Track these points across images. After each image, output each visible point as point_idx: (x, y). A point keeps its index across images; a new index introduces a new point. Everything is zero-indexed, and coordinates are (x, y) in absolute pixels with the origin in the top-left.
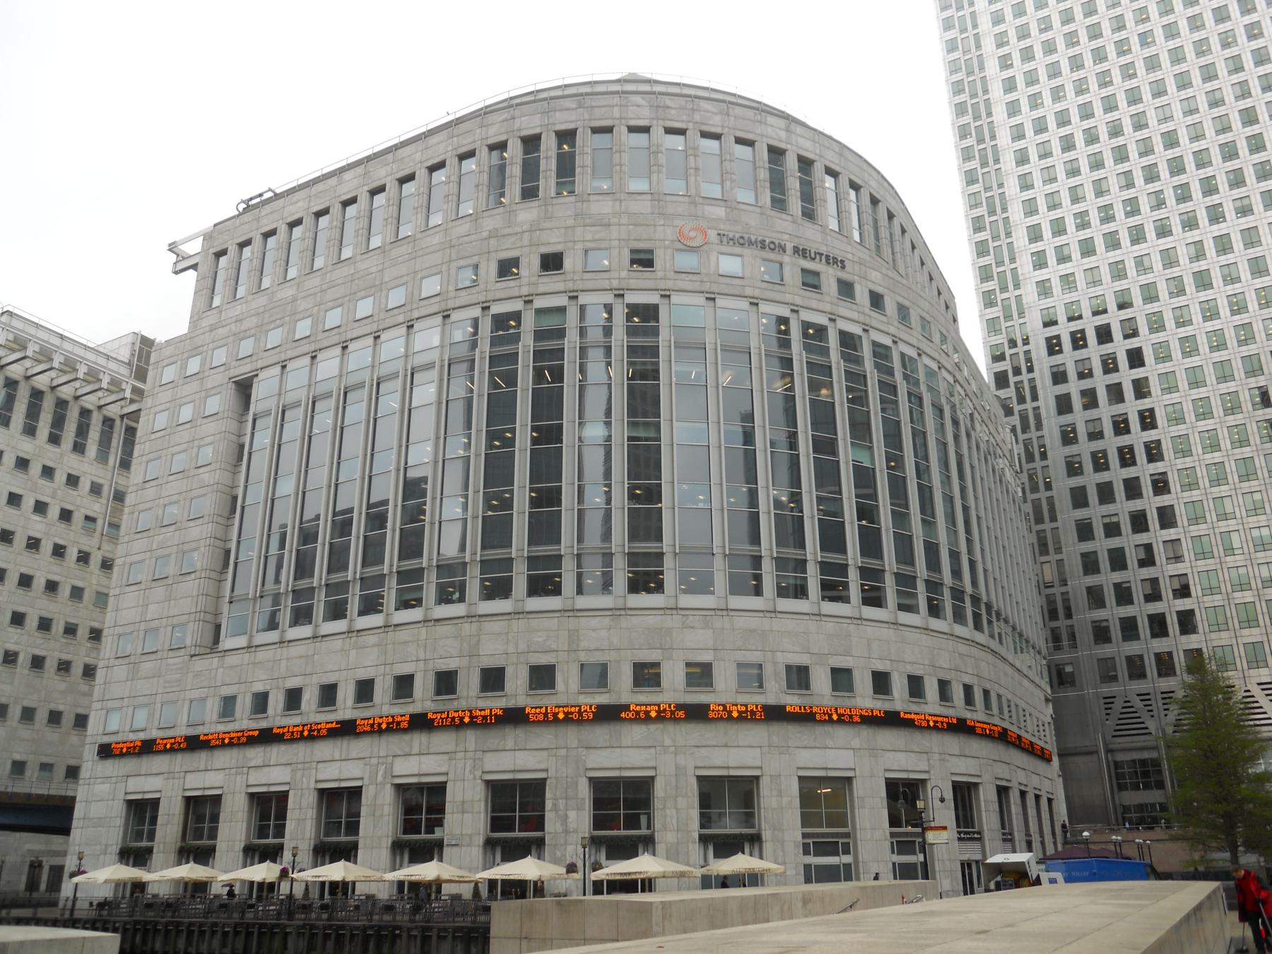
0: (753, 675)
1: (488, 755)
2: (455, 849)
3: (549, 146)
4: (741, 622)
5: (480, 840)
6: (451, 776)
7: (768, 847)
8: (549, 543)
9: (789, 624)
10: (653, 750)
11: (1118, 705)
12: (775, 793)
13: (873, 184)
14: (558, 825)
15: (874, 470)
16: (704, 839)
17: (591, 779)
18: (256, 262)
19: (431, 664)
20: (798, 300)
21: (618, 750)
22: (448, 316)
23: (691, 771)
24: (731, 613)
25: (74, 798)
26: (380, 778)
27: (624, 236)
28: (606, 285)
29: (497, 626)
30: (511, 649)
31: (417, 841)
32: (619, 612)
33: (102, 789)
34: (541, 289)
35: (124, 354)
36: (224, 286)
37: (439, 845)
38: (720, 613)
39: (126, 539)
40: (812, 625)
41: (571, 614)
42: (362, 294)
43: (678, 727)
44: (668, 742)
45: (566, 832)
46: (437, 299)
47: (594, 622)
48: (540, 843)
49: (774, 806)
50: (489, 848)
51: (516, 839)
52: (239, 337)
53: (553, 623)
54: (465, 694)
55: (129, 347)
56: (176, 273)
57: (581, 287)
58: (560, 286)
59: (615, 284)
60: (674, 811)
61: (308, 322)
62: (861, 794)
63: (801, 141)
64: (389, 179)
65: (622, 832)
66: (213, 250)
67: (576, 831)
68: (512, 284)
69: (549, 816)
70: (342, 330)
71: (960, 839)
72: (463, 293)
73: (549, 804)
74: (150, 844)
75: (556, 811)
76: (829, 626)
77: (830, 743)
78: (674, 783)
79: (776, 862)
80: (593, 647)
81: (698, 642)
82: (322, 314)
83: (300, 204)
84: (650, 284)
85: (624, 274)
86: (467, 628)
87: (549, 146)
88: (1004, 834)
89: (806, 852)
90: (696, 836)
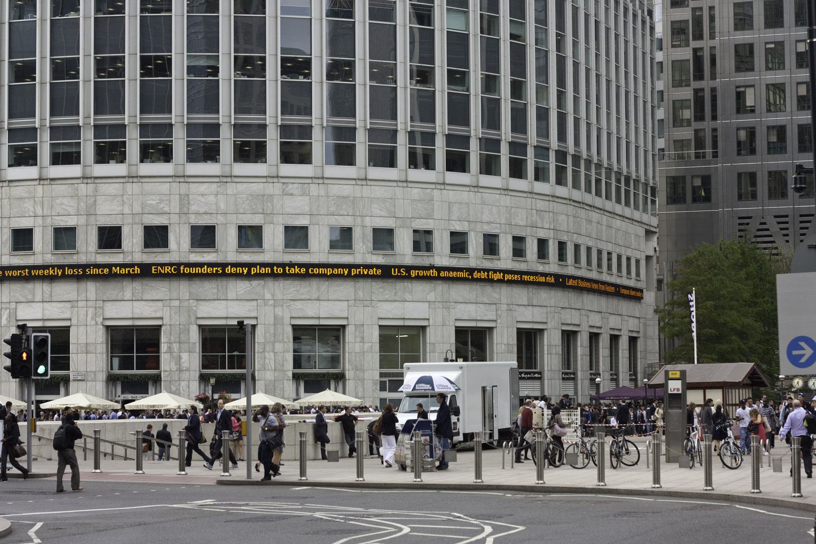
0: (423, 241)
1: (108, 304)
2: (80, 383)
4: (335, 189)
5: (102, 376)
6: (74, 321)
7: (350, 385)
8: (163, 112)
9: (379, 191)
10: (255, 303)
11: (754, 225)
12: (358, 340)
14: (173, 364)
15: (468, 35)
16: (296, 377)
17: (200, 326)
21: (225, 302)
23: (287, 321)
24: (326, 181)
29: (112, 188)
30: (127, 210)
37: (66, 380)
38: (316, 181)
40: (399, 192)
41: (182, 180)
43: (277, 283)
44: (268, 296)
45: (180, 370)
47: (203, 188)
48: (157, 379)
49: (357, 350)
50: (111, 384)
51: (135, 375)
53: (164, 188)
54: (84, 249)
60: (272, 354)
62: (433, 341)
65: (227, 371)
67: (188, 370)
69: (164, 358)
71: (563, 379)
73: (164, 347)
76: (415, 192)
77: (408, 296)
78: (272, 332)
79: (356, 397)
80: (202, 210)
81: (295, 208)
86: (83, 189)
88: (611, 375)
89: (383, 388)
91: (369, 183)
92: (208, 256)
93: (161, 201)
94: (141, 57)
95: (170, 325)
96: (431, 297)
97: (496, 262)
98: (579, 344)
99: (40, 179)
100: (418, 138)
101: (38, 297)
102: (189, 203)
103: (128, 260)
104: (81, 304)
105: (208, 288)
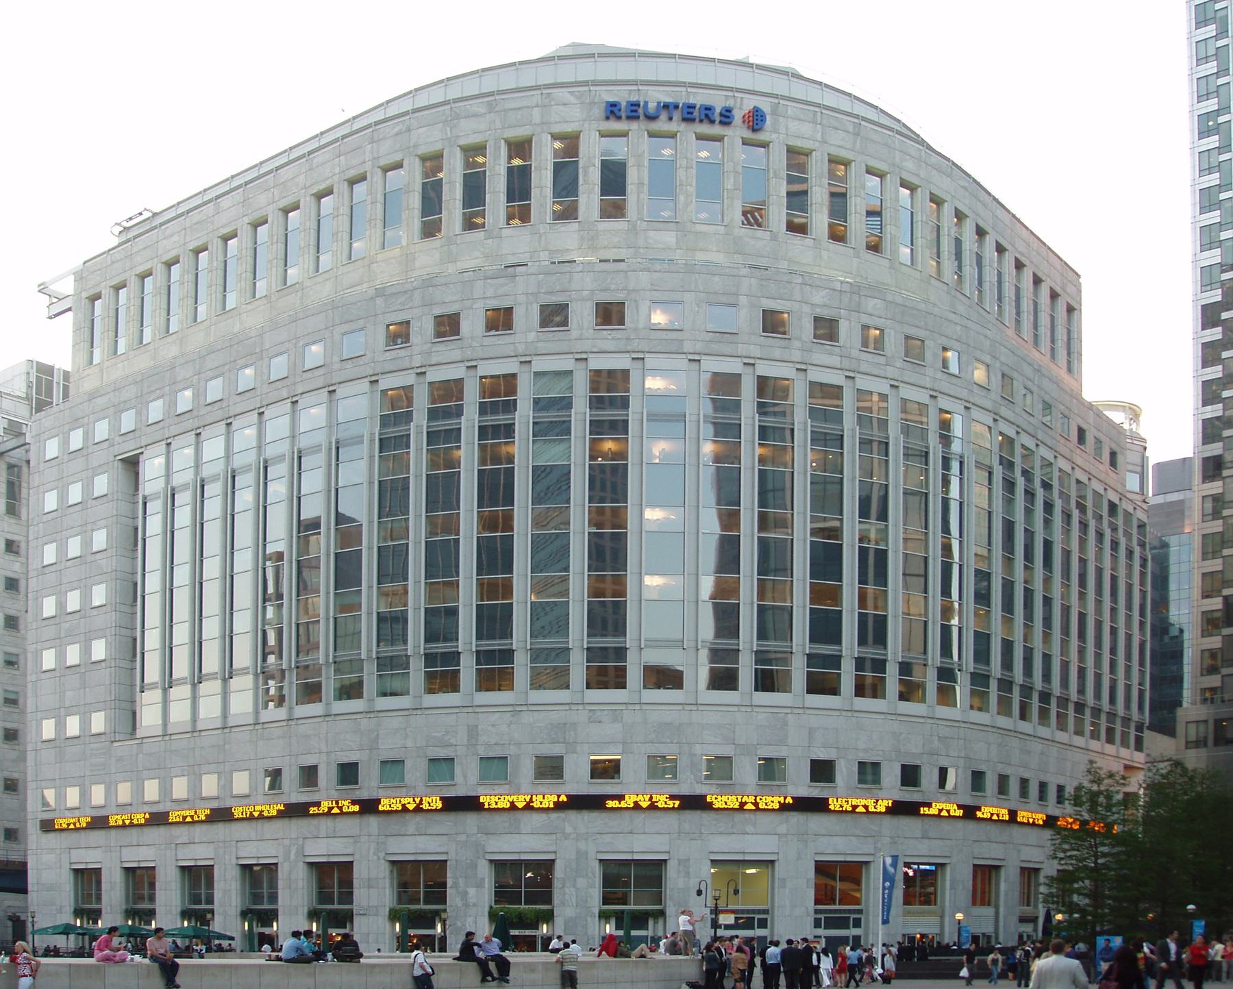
1: (391, 839)
10: (554, 837)
13: (910, 165)
18: (135, 311)
19: (333, 756)
20: (755, 351)
25: (25, 864)
26: (292, 857)
29: (395, 722)
30: (410, 744)
31: (416, 911)
32: (515, 710)
33: (49, 858)
34: (434, 360)
35: (20, 388)
36: (102, 339)
39: (34, 625)
42: (242, 362)
44: (569, 829)
45: (466, 905)
46: (321, 371)
52: (120, 408)
55: (24, 377)
56: (50, 318)
57: (481, 355)
58: (457, 355)
59: (521, 349)
61: (188, 393)
63: (794, 126)
64: (270, 209)
66: (84, 295)
68: (402, 353)
69: (450, 892)
70: (224, 404)
72: (349, 365)
77: (749, 829)
82: (202, 384)
83: (176, 238)
84: (564, 347)
85: (532, 336)
86: (365, 723)
91: (701, 708)
93: (447, 732)
96: (782, 829)
98: (1002, 879)
100: (868, 665)
101: (323, 834)
104: (364, 839)
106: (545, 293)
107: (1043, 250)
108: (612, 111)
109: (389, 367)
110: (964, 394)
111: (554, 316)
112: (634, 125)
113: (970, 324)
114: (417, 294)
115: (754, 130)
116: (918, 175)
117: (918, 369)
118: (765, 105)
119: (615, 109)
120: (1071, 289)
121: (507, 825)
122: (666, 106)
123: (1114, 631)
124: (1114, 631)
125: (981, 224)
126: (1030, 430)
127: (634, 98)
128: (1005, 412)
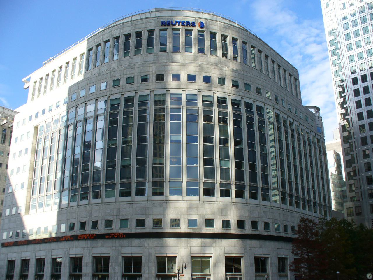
3: (145, 35)
5: (91, 275)
6: (84, 255)
10: (142, 248)
17: (123, 257)
21: (131, 247)
22: (86, 103)
23: (153, 254)
26: (66, 255)
27: (139, 71)
28: (133, 89)
34: (113, 92)
44: (146, 245)
45: (115, 273)
47: (125, 206)
58: (118, 91)
59: (136, 88)
60: (147, 267)
67: (117, 273)
69: (110, 268)
72: (91, 95)
74: (80, 273)
75: (112, 267)
85: (139, 85)
87: (145, 35)
90: (155, 275)
92: (126, 231)
94: (137, 158)
95: (112, 256)
97: (244, 231)
99: (148, 201)
101: (75, 247)
102: (120, 212)
103: (100, 233)
105: (125, 242)
106: (142, 72)
107: (286, 63)
108: (163, 23)
109: (101, 95)
110: (264, 101)
111: (144, 80)
112: (169, 27)
113: (264, 80)
114: (109, 74)
115: (201, 28)
116: (247, 40)
117: (249, 93)
118: (204, 21)
119: (164, 23)
120: (295, 74)
121: (128, 243)
122: (177, 22)
123: (313, 174)
124: (313, 174)
125: (267, 54)
126: (285, 112)
127: (169, 20)
128: (276, 106)
